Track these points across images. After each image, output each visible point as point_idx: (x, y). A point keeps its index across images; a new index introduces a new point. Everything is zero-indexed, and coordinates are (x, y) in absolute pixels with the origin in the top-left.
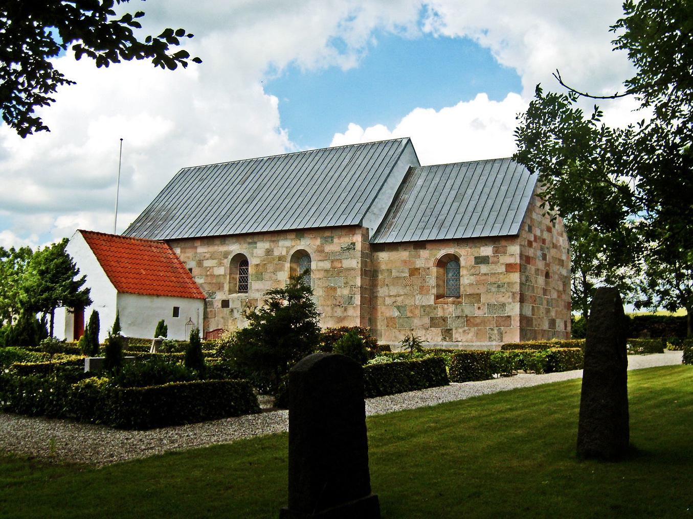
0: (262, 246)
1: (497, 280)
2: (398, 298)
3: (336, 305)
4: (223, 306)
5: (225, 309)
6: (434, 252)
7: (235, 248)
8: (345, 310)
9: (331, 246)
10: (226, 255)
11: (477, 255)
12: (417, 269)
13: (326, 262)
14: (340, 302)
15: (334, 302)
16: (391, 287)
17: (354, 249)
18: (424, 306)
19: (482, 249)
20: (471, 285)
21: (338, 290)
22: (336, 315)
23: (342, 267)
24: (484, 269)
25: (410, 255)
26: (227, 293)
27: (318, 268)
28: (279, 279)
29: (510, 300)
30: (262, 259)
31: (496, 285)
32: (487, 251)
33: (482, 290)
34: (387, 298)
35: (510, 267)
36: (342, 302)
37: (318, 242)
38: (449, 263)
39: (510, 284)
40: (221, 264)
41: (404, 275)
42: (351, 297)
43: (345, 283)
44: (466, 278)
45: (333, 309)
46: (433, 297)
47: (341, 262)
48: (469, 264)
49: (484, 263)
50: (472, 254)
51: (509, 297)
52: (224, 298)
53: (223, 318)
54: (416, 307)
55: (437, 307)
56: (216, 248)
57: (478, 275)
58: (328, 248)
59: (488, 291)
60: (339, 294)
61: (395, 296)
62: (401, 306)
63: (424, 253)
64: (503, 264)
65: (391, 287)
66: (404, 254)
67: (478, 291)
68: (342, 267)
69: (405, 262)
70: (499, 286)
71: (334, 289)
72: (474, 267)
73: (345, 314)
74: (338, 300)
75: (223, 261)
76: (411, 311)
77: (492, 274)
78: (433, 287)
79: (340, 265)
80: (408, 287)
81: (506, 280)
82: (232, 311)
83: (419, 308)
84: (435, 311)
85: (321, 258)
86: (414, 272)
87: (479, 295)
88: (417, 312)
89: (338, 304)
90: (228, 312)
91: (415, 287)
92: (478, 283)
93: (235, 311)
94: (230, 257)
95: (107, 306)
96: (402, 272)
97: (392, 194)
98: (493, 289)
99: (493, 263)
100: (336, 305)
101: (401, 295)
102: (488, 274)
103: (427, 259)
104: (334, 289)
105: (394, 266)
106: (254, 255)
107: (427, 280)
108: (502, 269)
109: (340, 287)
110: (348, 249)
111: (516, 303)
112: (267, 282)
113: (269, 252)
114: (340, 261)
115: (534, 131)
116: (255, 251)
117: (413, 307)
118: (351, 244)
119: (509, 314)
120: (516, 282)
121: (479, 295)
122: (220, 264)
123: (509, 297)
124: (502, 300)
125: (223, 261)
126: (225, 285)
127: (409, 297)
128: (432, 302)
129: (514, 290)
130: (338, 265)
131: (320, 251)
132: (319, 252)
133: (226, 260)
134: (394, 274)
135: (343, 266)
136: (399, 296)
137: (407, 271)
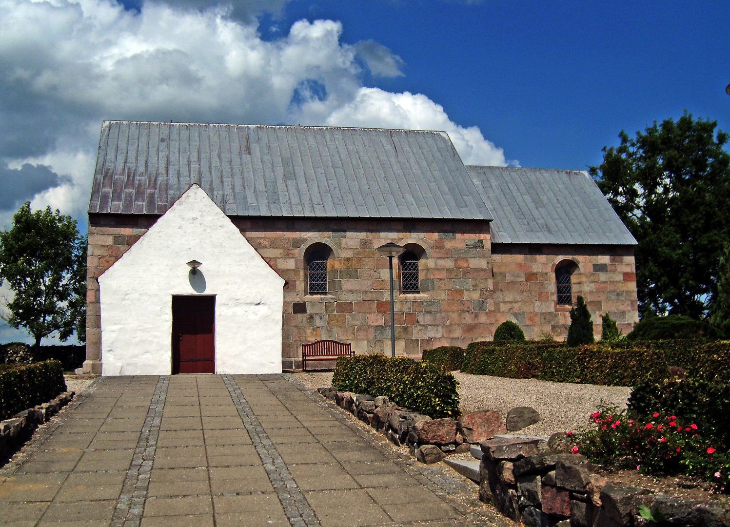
0: (353, 239)
1: (616, 288)
2: (514, 305)
3: (463, 311)
4: (295, 312)
5: (300, 315)
6: (551, 257)
7: (313, 237)
8: (476, 316)
9: (453, 242)
10: (296, 244)
11: (595, 262)
12: (534, 273)
13: (448, 260)
14: (469, 308)
15: (462, 308)
16: (506, 293)
17: (483, 247)
18: (544, 313)
19: (600, 257)
20: (591, 292)
21: (466, 293)
22: (464, 322)
23: (468, 267)
24: (603, 277)
25: (525, 259)
26: (302, 293)
27: (439, 267)
28: (383, 278)
29: (629, 308)
30: (356, 251)
31: (616, 293)
32: (605, 259)
33: (602, 298)
34: (502, 305)
35: (627, 276)
36: (471, 308)
37: (436, 236)
38: (564, 271)
39: (628, 292)
40: (288, 255)
41: (519, 280)
42: (483, 302)
43: (473, 286)
44: (585, 285)
45: (460, 315)
46: (553, 304)
47: (467, 261)
48: (588, 271)
49: (602, 271)
50: (590, 261)
51: (628, 305)
52: (297, 300)
53: (296, 326)
54: (536, 314)
55: (558, 315)
56: (279, 234)
57: (597, 282)
58: (448, 245)
59: (608, 299)
60: (467, 298)
61: (511, 302)
62: (519, 313)
63: (541, 258)
64: (620, 273)
65: (506, 293)
66: (520, 258)
67: (598, 299)
68: (468, 267)
69: (520, 265)
70: (618, 295)
71: (460, 292)
72: (592, 274)
73: (476, 322)
74: (466, 306)
75: (291, 252)
76: (531, 319)
77: (610, 282)
78: (552, 294)
79: (466, 265)
80: (525, 293)
81: (625, 289)
82: (311, 317)
83: (539, 315)
84: (556, 319)
85: (440, 255)
86: (531, 276)
87: (599, 303)
88: (537, 319)
89: (466, 309)
90: (305, 319)
91: (533, 293)
92: (598, 291)
93: (317, 319)
94: (304, 247)
95: (265, 304)
96: (518, 276)
97: (367, 215)
98: (613, 297)
99: (611, 271)
100: (463, 311)
101: (518, 302)
102: (607, 282)
103: (545, 264)
104: (460, 292)
105: (508, 270)
106: (343, 246)
107: (546, 286)
108: (620, 278)
109: (467, 290)
110: (475, 247)
111: (635, 311)
112: (366, 282)
113: (364, 243)
114: (466, 259)
115: (624, 156)
116: (344, 241)
117: (532, 315)
118: (479, 241)
119: (629, 322)
120: (633, 291)
121: (599, 303)
122: (288, 255)
123: (628, 305)
124: (622, 308)
125: (291, 252)
126: (298, 283)
127: (527, 304)
128: (552, 309)
129: (632, 299)
130: (462, 264)
131: (439, 246)
132: (437, 247)
133: (297, 251)
134: (509, 278)
135: (470, 266)
136: (516, 302)
137: (523, 275)
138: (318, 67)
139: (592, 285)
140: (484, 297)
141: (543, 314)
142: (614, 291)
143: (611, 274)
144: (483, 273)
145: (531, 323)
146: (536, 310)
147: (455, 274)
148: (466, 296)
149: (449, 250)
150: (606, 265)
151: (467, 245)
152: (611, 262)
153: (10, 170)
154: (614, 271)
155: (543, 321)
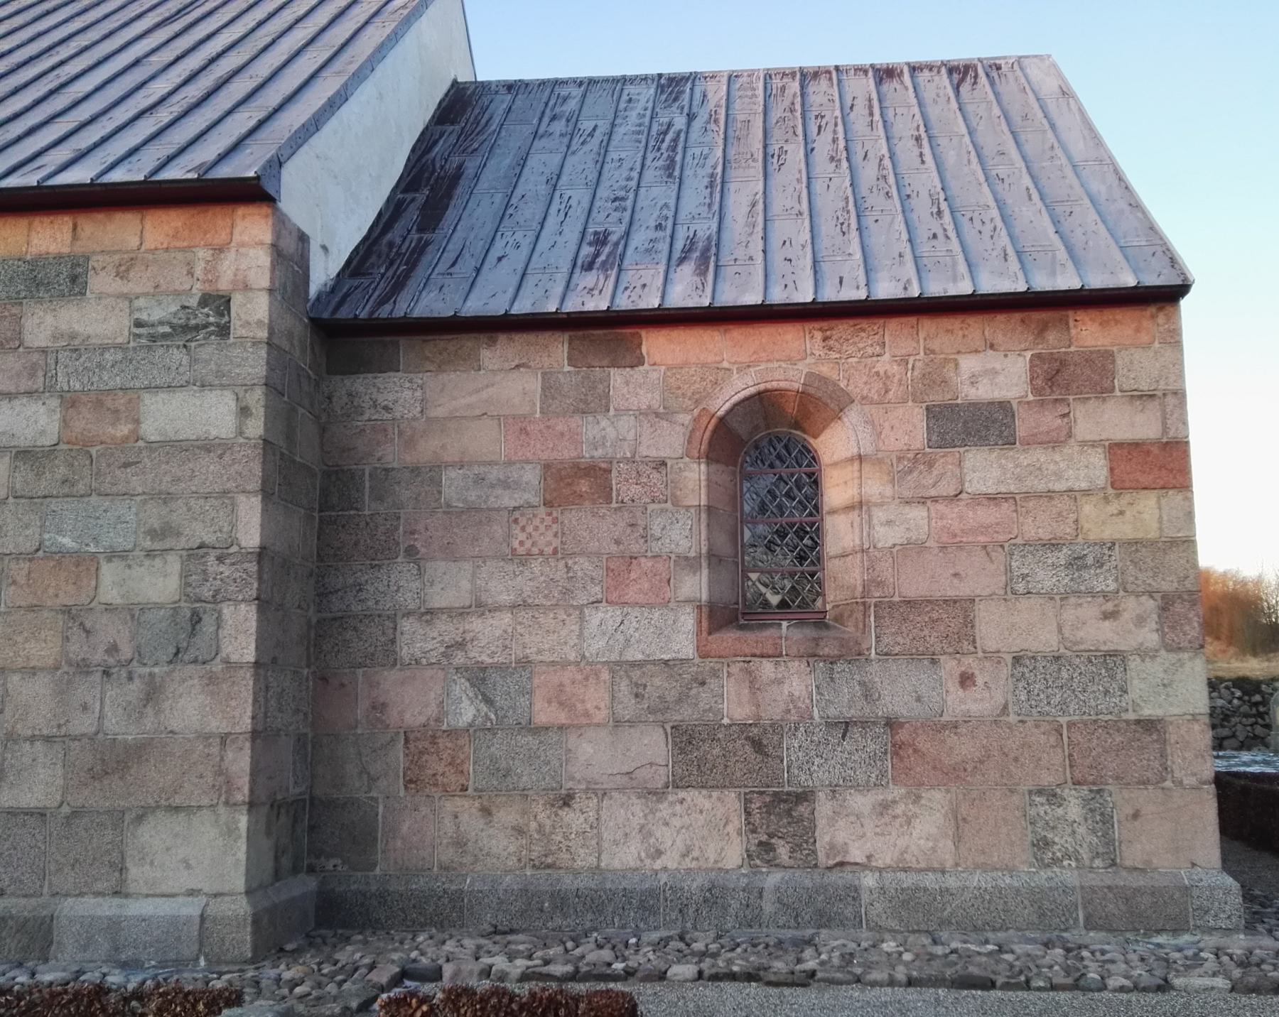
3: (83, 668)
8: (153, 693)
14: (113, 649)
15: (77, 649)
18: (634, 664)
24: (983, 469)
29: (1149, 636)
31: (1063, 556)
46: (688, 620)
51: (1140, 621)
62: (501, 668)
80: (536, 566)
89: (99, 656)
104: (83, 564)
108: (1096, 468)
118: (205, 300)
121: (964, 607)
124: (1102, 634)
138: (1246, 584)
139: (917, 514)
140: (207, 593)
141: (621, 667)
142: (1053, 545)
143: (1038, 456)
144: (208, 467)
145: (562, 718)
146: (595, 646)
147: (62, 471)
148: (111, 584)
149: (44, 351)
150: (1004, 407)
151: (139, 324)
152: (1037, 391)
153: (1214, 592)
154: (1054, 442)
155: (628, 707)
